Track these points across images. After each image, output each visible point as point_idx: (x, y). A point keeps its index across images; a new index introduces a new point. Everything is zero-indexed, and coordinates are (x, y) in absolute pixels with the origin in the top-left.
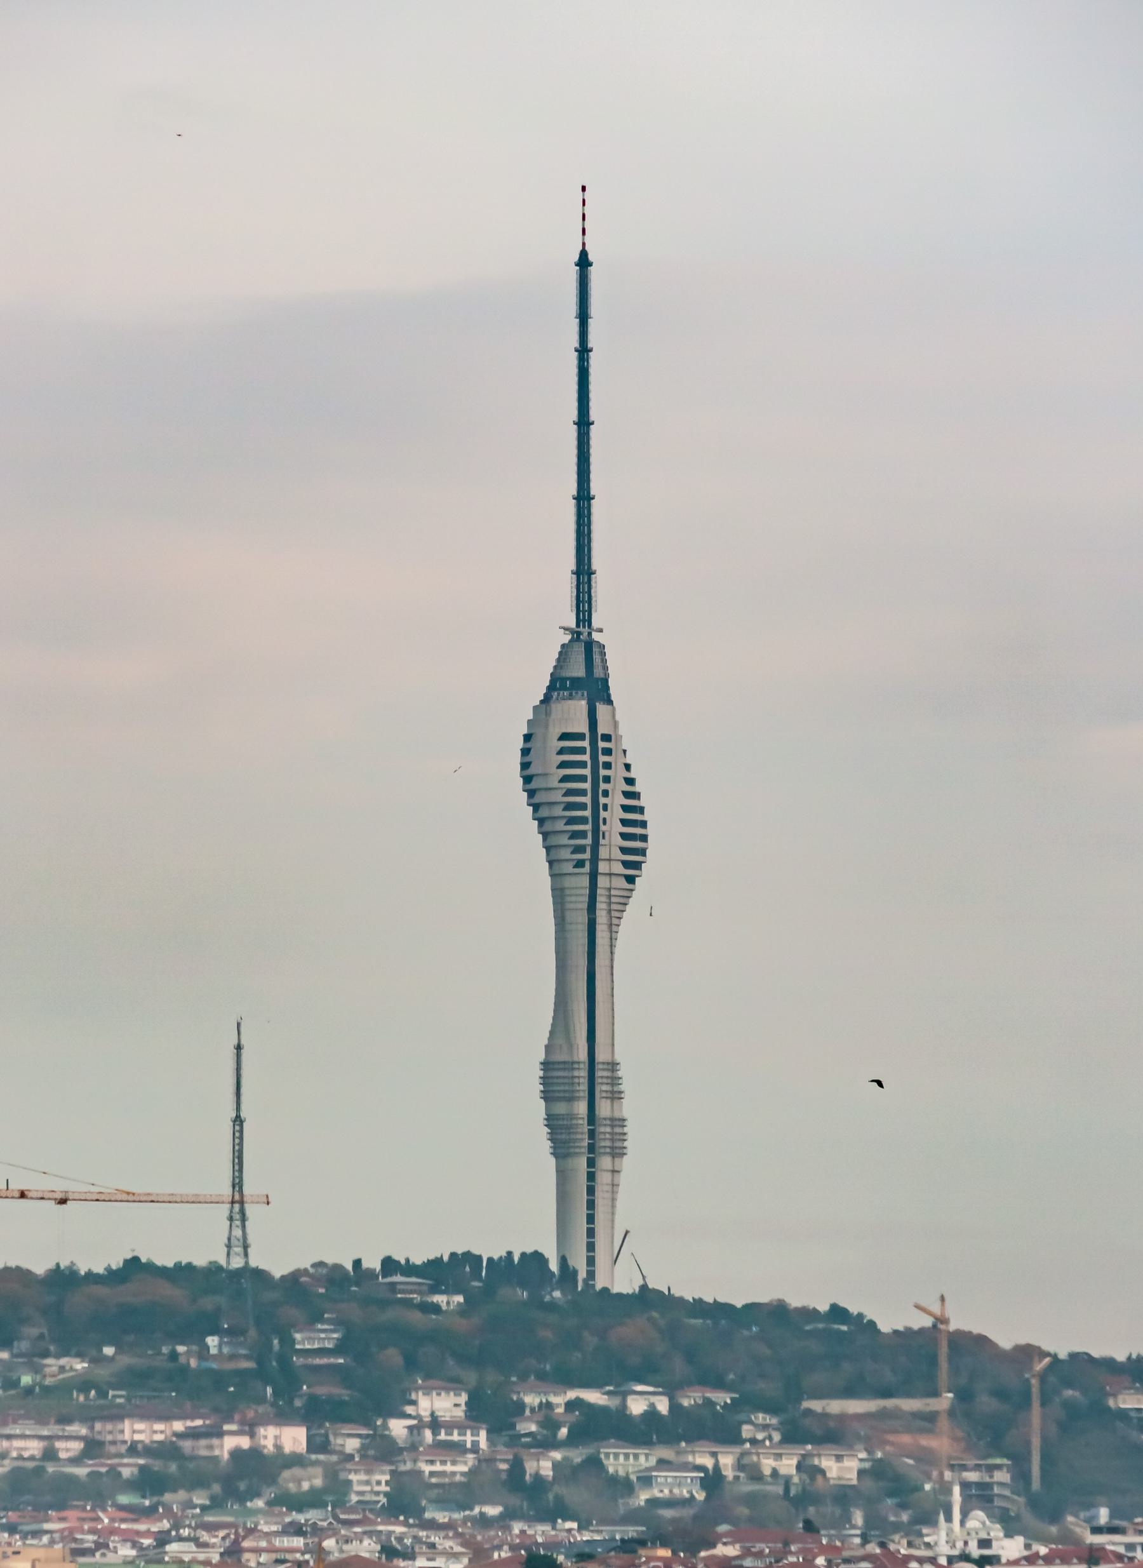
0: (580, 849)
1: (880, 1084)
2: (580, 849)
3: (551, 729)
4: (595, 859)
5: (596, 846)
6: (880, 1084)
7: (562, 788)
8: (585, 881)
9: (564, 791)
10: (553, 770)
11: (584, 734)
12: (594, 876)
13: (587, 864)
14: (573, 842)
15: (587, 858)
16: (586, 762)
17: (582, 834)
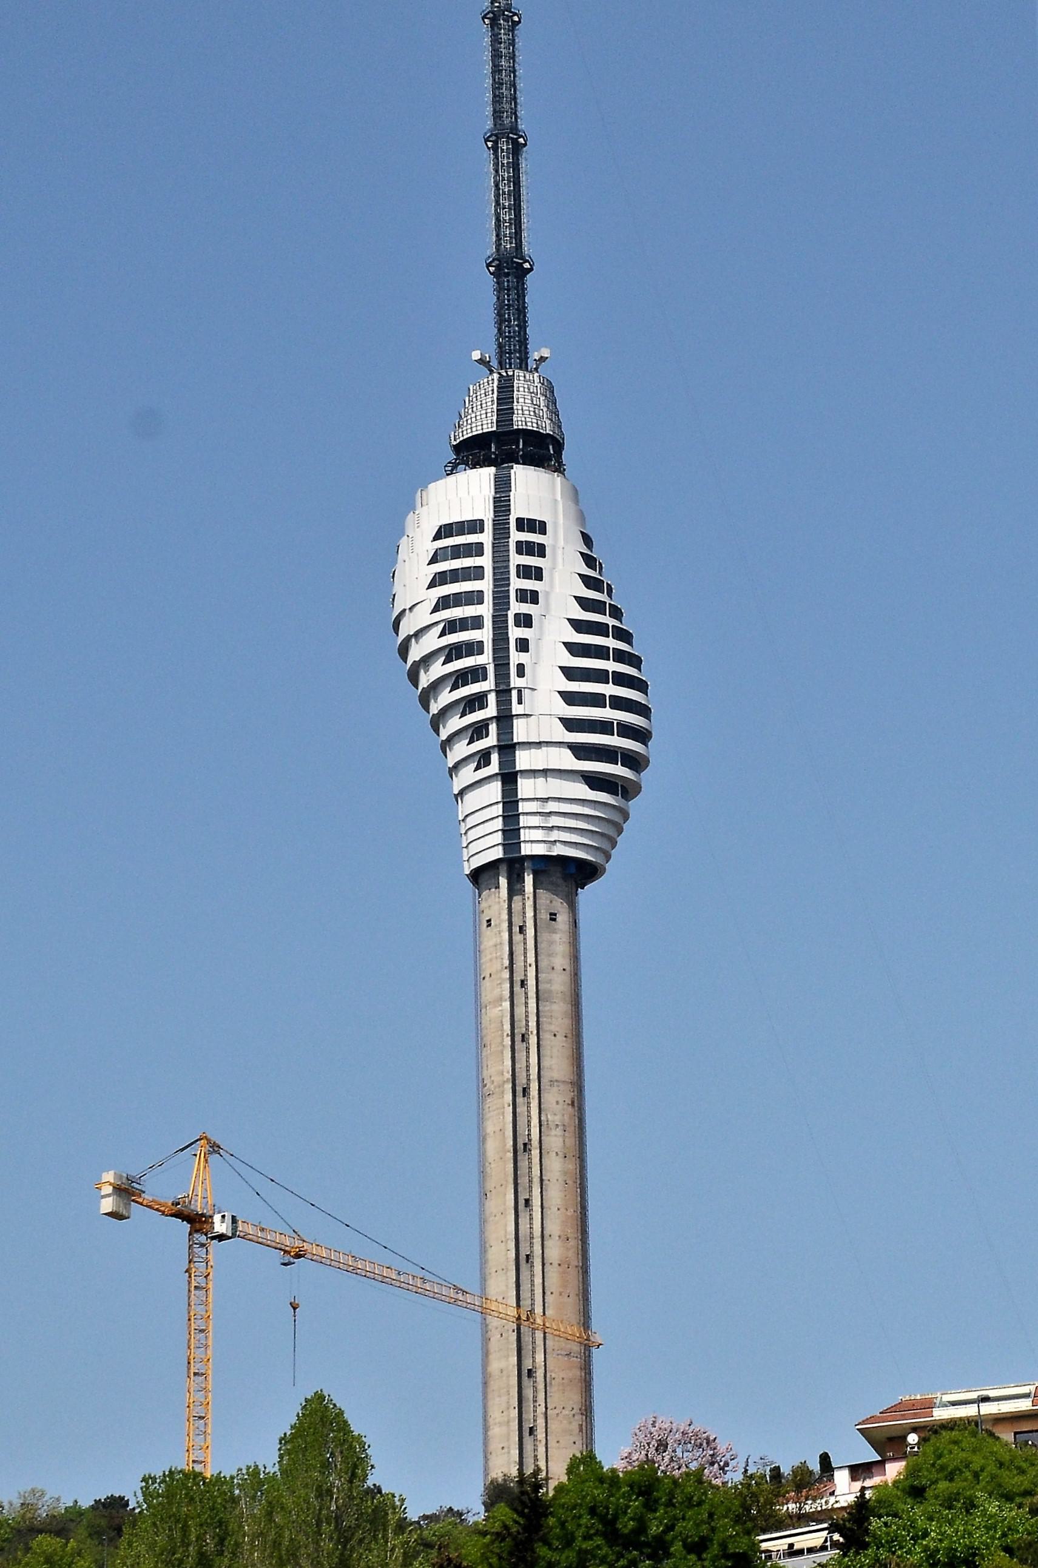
4: (507, 748)
5: (505, 719)
7: (437, 623)
8: (494, 791)
12: (509, 778)
13: (493, 728)
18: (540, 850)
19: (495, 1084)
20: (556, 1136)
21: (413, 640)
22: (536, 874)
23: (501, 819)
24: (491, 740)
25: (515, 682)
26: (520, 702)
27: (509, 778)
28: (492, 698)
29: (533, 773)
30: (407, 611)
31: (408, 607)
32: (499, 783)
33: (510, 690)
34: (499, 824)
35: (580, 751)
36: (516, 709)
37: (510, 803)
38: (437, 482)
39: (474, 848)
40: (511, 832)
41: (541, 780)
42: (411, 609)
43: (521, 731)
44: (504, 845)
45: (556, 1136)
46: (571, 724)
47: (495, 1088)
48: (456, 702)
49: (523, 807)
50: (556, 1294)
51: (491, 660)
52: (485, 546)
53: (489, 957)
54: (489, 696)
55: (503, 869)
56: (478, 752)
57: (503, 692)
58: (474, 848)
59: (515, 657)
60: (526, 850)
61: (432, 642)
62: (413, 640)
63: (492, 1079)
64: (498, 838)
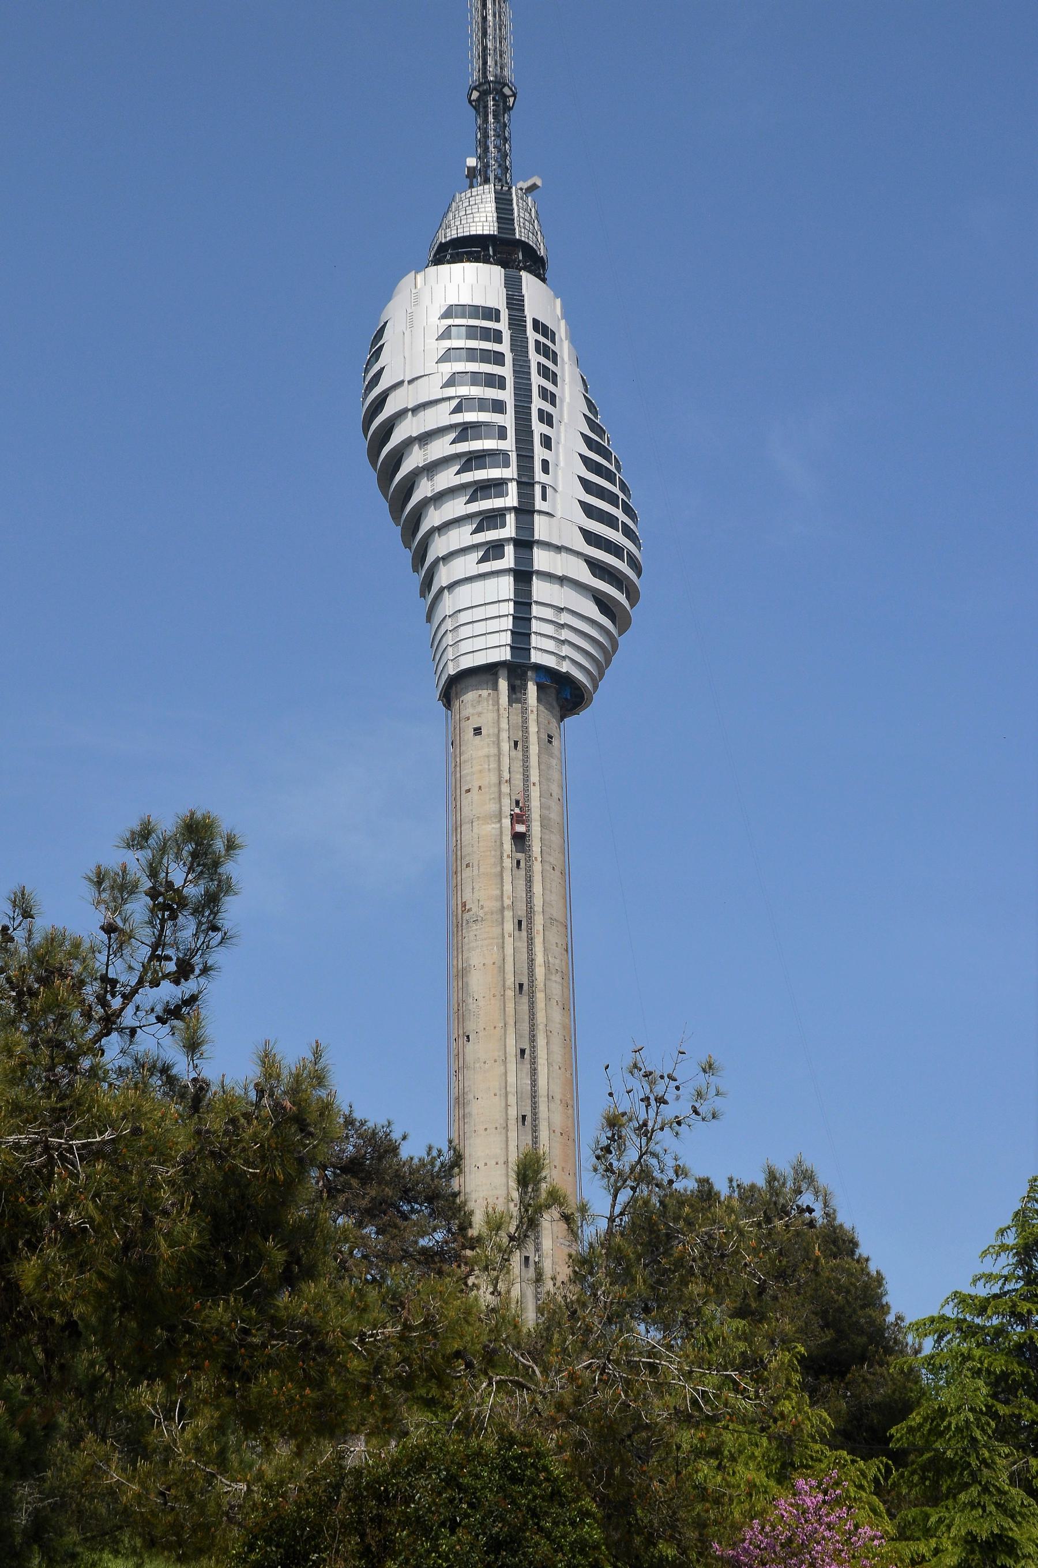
0: (492, 519)
1: (607, 1067)
2: (492, 519)
3: (425, 300)
4: (524, 544)
5: (525, 511)
6: (607, 1067)
7: (449, 399)
8: (506, 586)
9: (454, 403)
10: (431, 366)
11: (498, 311)
12: (523, 576)
13: (511, 519)
14: (468, 477)
15: (508, 536)
16: (505, 454)
17: (496, 487)
18: (550, 662)
19: (486, 909)
20: (556, 981)
21: (410, 413)
22: (540, 687)
23: (511, 618)
24: (509, 530)
25: (539, 475)
26: (544, 498)
27: (523, 576)
28: (513, 488)
29: (549, 576)
30: (406, 383)
31: (408, 378)
32: (512, 579)
33: (532, 485)
34: (508, 623)
35: (597, 568)
36: (539, 504)
37: (523, 604)
38: (440, 267)
39: (464, 647)
40: (521, 635)
41: (556, 587)
42: (410, 382)
43: (541, 528)
44: (512, 648)
45: (556, 981)
46: (591, 538)
47: (486, 914)
48: (462, 487)
49: (536, 610)
50: (559, 1168)
51: (514, 449)
52: (504, 335)
53: (476, 768)
54: (510, 484)
55: (503, 674)
56: (487, 543)
57: (526, 485)
58: (464, 647)
59: (539, 453)
60: (536, 657)
61: (441, 416)
62: (410, 413)
63: (481, 903)
64: (507, 638)
